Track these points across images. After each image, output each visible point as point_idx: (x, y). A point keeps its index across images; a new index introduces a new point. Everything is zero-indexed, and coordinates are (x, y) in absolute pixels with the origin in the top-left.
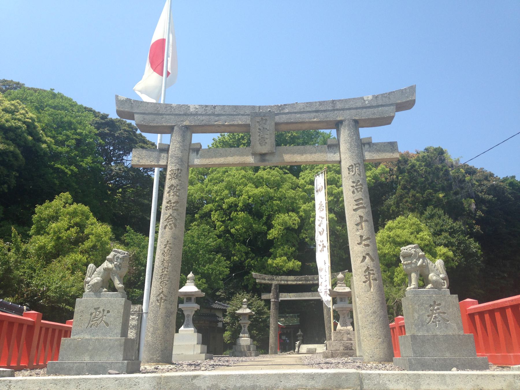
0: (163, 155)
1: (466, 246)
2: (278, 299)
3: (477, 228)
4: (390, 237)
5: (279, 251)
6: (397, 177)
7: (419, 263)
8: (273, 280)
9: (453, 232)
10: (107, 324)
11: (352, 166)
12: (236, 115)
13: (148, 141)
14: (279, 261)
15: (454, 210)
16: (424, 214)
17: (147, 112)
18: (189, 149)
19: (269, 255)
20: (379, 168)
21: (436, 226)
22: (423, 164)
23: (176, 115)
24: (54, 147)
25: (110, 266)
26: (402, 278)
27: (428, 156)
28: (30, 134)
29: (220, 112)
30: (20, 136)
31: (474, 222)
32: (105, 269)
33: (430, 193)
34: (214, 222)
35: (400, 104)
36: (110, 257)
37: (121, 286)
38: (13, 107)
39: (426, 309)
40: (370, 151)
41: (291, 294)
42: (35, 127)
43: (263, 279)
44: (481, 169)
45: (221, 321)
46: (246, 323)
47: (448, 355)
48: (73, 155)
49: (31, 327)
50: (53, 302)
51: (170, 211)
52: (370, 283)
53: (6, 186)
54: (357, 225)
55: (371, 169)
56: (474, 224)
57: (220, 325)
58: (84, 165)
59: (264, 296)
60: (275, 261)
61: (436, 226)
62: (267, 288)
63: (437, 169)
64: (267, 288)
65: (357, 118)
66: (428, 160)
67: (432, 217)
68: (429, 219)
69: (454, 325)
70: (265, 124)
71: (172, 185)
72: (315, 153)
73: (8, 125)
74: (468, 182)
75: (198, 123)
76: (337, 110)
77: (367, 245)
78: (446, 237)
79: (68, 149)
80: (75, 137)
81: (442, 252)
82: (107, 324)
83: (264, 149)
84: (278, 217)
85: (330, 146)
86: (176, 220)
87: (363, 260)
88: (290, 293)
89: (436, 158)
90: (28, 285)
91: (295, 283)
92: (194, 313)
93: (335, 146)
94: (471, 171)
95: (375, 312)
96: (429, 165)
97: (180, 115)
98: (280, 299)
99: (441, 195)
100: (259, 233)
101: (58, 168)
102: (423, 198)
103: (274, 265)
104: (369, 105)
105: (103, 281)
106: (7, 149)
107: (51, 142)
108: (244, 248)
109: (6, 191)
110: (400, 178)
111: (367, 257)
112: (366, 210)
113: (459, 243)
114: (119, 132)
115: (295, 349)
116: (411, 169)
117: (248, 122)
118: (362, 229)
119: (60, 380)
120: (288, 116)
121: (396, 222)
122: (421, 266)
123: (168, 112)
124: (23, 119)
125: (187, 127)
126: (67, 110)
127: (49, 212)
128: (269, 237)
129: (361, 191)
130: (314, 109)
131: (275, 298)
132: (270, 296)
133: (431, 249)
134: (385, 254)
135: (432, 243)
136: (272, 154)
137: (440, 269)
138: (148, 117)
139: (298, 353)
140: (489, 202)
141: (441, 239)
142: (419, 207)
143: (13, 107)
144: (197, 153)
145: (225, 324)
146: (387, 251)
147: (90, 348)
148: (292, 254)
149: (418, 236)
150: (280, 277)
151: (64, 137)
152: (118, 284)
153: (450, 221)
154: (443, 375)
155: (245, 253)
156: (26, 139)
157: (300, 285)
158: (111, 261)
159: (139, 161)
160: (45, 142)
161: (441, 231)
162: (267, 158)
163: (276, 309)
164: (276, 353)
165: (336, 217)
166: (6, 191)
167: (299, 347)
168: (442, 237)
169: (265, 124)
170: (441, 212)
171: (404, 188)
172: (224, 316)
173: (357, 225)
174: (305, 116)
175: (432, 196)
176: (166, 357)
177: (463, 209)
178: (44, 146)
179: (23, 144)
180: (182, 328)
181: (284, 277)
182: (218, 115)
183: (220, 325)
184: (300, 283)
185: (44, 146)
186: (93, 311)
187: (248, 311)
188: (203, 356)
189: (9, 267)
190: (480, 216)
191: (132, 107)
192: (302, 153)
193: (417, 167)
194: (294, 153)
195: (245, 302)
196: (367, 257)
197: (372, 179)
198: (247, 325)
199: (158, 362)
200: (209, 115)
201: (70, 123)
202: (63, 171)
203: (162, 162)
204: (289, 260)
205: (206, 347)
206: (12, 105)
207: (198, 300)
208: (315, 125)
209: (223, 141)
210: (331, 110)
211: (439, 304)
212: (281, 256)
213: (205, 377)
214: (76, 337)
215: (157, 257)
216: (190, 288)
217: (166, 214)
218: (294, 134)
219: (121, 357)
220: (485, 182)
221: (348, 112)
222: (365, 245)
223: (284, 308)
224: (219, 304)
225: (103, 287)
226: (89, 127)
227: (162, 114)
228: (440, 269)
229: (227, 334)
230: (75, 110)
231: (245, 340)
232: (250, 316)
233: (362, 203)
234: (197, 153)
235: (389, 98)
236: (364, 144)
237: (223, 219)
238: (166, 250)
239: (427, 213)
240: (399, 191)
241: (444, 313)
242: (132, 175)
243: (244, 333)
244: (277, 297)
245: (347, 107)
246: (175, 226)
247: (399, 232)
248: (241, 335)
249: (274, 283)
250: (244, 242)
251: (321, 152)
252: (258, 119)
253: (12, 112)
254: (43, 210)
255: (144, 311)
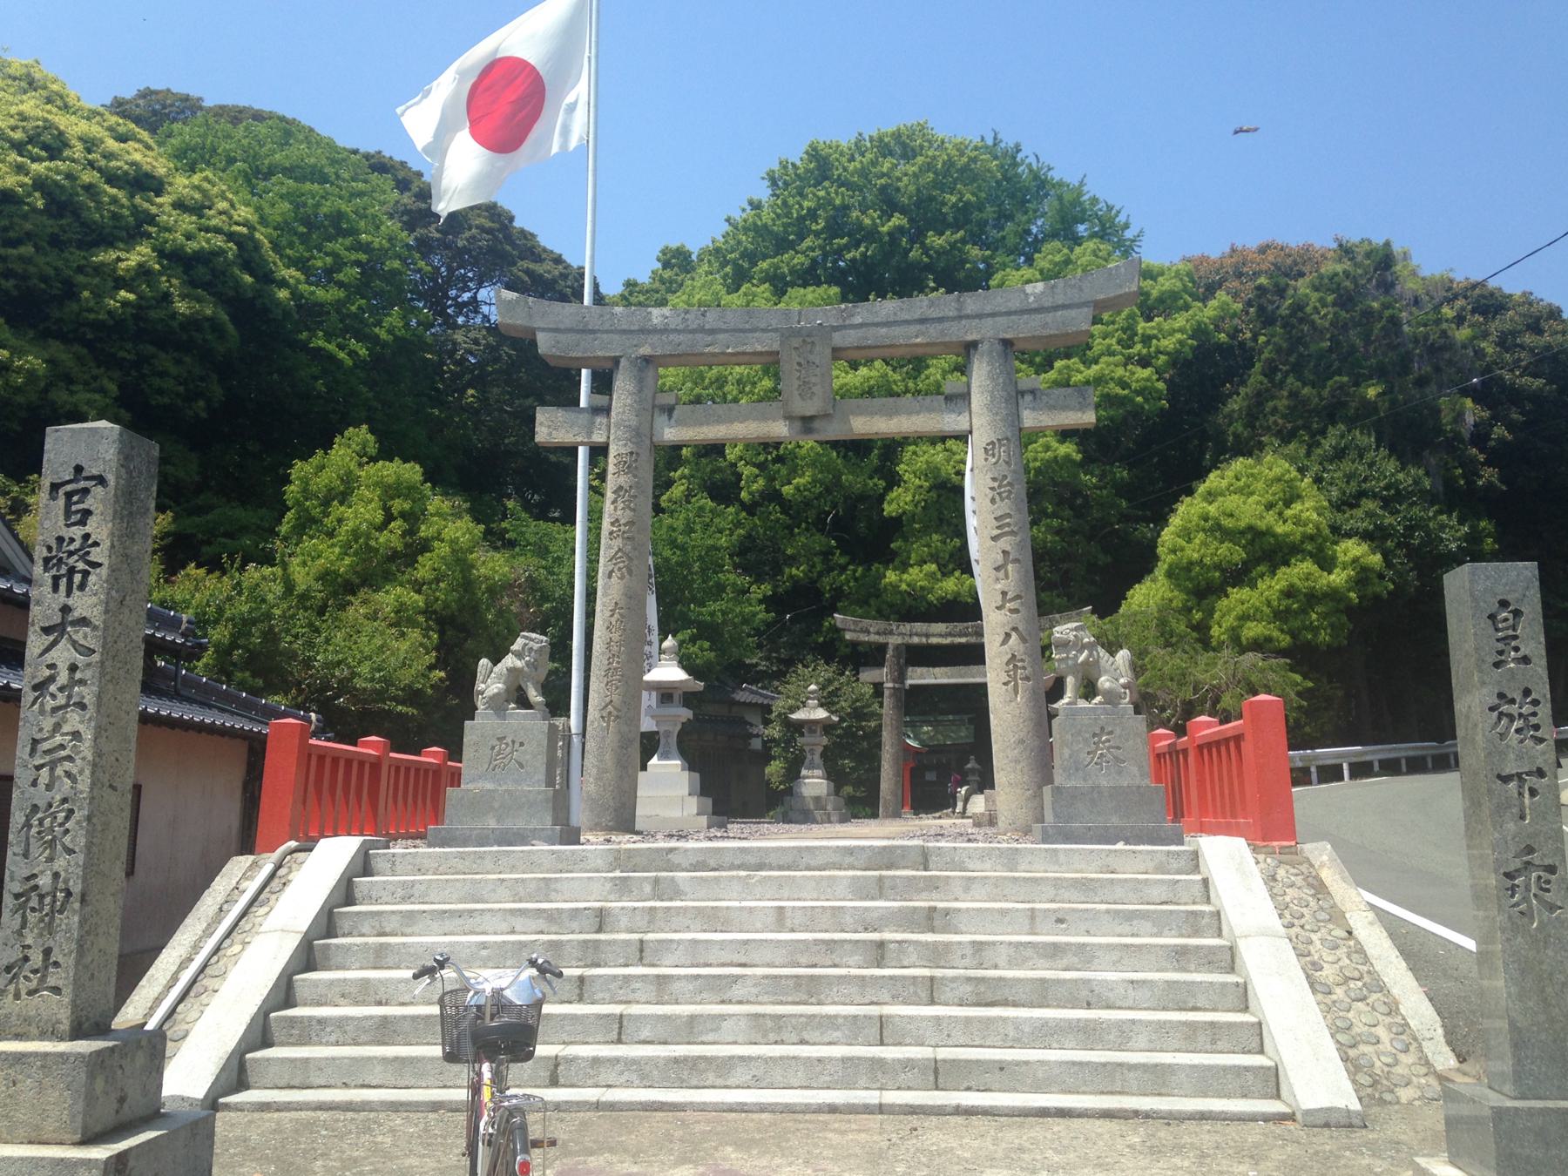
0: (600, 420)
1: (1428, 534)
2: (903, 683)
3: (1489, 475)
4: (1206, 520)
5: (918, 549)
6: (1255, 338)
7: (1081, 659)
8: (891, 633)
9: (1392, 499)
10: (521, 766)
11: (992, 443)
12: (751, 331)
13: (545, 250)
14: (916, 576)
15: (1408, 433)
16: (1319, 444)
17: (562, 326)
18: (654, 407)
19: (888, 558)
20: (1213, 303)
21: (1348, 483)
22: (1330, 299)
23: (624, 332)
24: (303, 287)
25: (519, 664)
26: (1233, 629)
27: (1347, 274)
28: (247, 266)
29: (715, 325)
30: (223, 273)
31: (1481, 458)
32: (511, 670)
33: (1341, 387)
34: (734, 465)
35: (1103, 301)
36: (516, 647)
37: (540, 699)
38: (197, 196)
39: (1085, 740)
40: (1033, 409)
41: (937, 670)
42: (257, 246)
43: (862, 631)
44: (1524, 294)
45: (757, 736)
46: (816, 743)
47: (1115, 821)
48: (353, 308)
49: (376, 765)
50: (365, 702)
51: (618, 543)
52: (1016, 686)
53: (201, 403)
54: (997, 569)
55: (1187, 308)
56: (1483, 464)
57: (756, 744)
58: (383, 335)
59: (868, 675)
60: (905, 576)
61: (1348, 483)
62: (872, 656)
63: (1368, 314)
64: (872, 656)
65: (1008, 336)
66: (1345, 288)
67: (1339, 454)
68: (1331, 462)
69: (1135, 770)
70: (811, 352)
71: (621, 488)
72: (918, 413)
73: (192, 246)
74: (1464, 347)
75: (668, 350)
76: (968, 317)
77: (1015, 611)
78: (1370, 515)
79: (342, 294)
80: (354, 256)
81: (1351, 555)
82: (521, 766)
83: (809, 409)
84: (915, 453)
85: (949, 398)
86: (630, 559)
87: (1004, 642)
88: (934, 666)
89: (1369, 280)
90: (307, 663)
91: (948, 641)
92: (679, 727)
93: (961, 399)
94: (1488, 304)
95: (1021, 741)
96: (1346, 300)
97: (631, 332)
98: (909, 682)
99: (1372, 392)
100: (862, 497)
101: (320, 349)
102: (1322, 399)
103: (904, 587)
104: (1035, 306)
105: (507, 691)
106: (198, 312)
107: (298, 282)
108: (819, 541)
109: (204, 415)
110: (1262, 339)
111: (1014, 635)
112: (1018, 538)
113: (1406, 528)
114: (467, 234)
115: (955, 806)
116: (1291, 316)
117: (776, 347)
118: (1007, 577)
119: (469, 853)
120: (860, 333)
121: (1230, 473)
122: (1086, 662)
123: (607, 326)
124: (226, 228)
125: (647, 360)
126: (324, 179)
127: (327, 479)
128: (889, 509)
129: (1008, 497)
130: (916, 316)
131: (894, 681)
132: (883, 674)
133: (1321, 549)
134: (1191, 563)
135: (1327, 531)
136: (826, 416)
137: (1122, 669)
138: (563, 338)
139: (963, 814)
140: (1536, 397)
141: (1356, 519)
142: (1303, 427)
143: (197, 196)
144: (670, 416)
145: (769, 743)
146: (1196, 555)
147: (496, 805)
148: (951, 556)
149: (1289, 513)
150: (908, 626)
151: (329, 260)
152: (534, 696)
153: (1391, 466)
154: (1055, 850)
155: (821, 553)
156: (238, 284)
157: (960, 644)
158: (519, 655)
159: (550, 434)
160: (283, 284)
161: (1362, 494)
162: (816, 424)
163: (896, 707)
164: (896, 815)
165: (1079, 452)
166: (204, 415)
167: (966, 800)
168: (1359, 513)
169: (811, 352)
170: (1366, 440)
171: (1270, 371)
172: (767, 723)
173: (997, 569)
174: (897, 331)
175: (1348, 394)
176: (623, 819)
177: (1439, 430)
178: (283, 294)
179: (231, 293)
180: (654, 760)
181: (919, 626)
182: (712, 332)
183: (756, 744)
184: (963, 640)
185: (283, 294)
186: (496, 742)
187: (821, 714)
188: (704, 820)
189: (271, 628)
190: (1501, 440)
191: (530, 316)
192: (891, 413)
193: (1309, 309)
194: (872, 414)
195: (812, 692)
196: (1014, 635)
197: (1192, 337)
198: (820, 749)
199: (610, 829)
200: (693, 331)
201: (339, 216)
202: (331, 358)
203: (599, 438)
204: (944, 575)
205: (709, 802)
206: (197, 188)
207: (689, 699)
208: (920, 351)
209: (755, 224)
210: (953, 319)
211: (1111, 733)
212: (922, 562)
213: (686, 850)
214: (470, 786)
215: (597, 633)
216: (669, 672)
217: (610, 547)
218: (968, 196)
219: (549, 819)
220: (1528, 339)
221: (990, 321)
222: (1011, 611)
223: (917, 702)
224: (752, 692)
225: (508, 701)
226: (392, 226)
227: (593, 332)
228: (1122, 669)
229: (774, 769)
230: (346, 176)
231: (814, 783)
232: (827, 727)
233: (1008, 525)
234: (670, 416)
235: (1081, 289)
236: (1023, 393)
237: (762, 458)
238: (613, 620)
239: (1328, 443)
240: (1256, 377)
241: (1118, 748)
242: (509, 356)
243: (812, 767)
244: (901, 677)
245: (988, 309)
246: (630, 572)
247: (1232, 502)
248: (804, 772)
249: (894, 640)
250: (819, 525)
251: (930, 410)
252: (796, 342)
253: (197, 210)
254: (308, 475)
255: (574, 731)
